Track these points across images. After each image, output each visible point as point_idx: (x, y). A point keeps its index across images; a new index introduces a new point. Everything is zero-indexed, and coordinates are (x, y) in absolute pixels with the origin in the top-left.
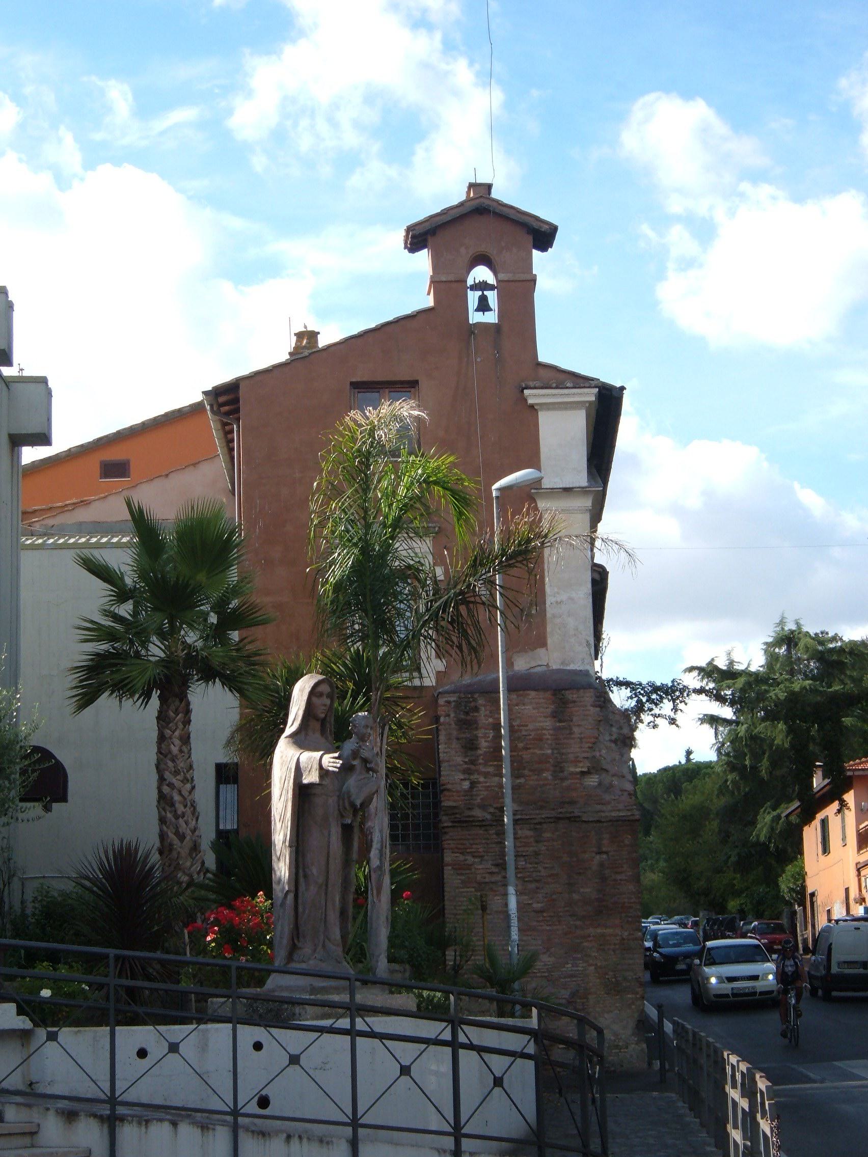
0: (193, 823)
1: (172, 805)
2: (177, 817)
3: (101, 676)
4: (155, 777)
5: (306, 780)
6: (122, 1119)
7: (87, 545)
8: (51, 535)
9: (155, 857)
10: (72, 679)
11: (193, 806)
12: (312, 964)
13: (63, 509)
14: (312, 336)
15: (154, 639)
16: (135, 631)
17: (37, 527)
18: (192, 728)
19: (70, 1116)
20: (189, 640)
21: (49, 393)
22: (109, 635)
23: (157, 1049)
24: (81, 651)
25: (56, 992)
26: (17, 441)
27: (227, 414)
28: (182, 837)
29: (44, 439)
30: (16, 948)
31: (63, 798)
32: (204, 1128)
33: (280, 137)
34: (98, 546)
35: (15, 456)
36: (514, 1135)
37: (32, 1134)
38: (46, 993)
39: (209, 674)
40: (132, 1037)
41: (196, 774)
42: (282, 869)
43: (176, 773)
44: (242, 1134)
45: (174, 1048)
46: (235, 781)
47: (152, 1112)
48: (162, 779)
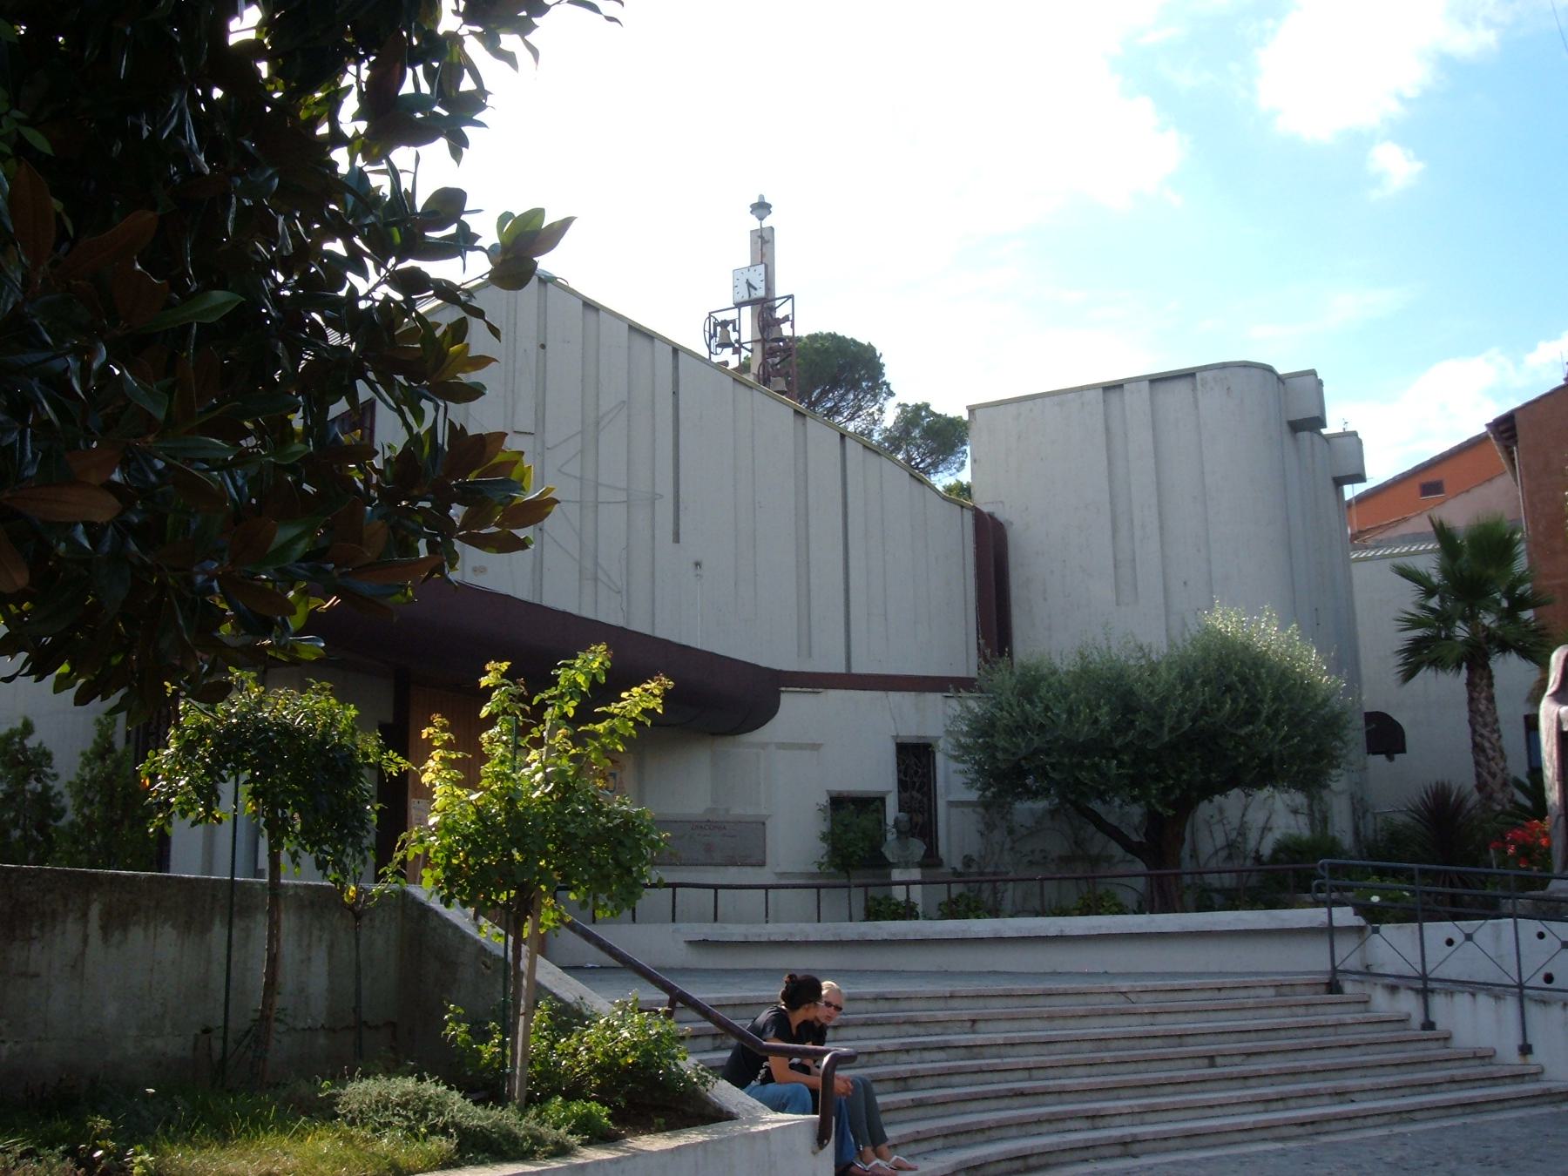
0: (1502, 765)
1: (1483, 750)
2: (1489, 760)
3: (1420, 655)
4: (1468, 729)
6: (1432, 991)
9: (1476, 796)
15: (1459, 623)
16: (1443, 618)
17: (1369, 542)
18: (1497, 690)
19: (1393, 989)
21: (1360, 442)
22: (1415, 623)
23: (1458, 938)
25: (1383, 898)
26: (1339, 482)
27: (1508, 439)
28: (1494, 776)
29: (1360, 478)
31: (1403, 750)
32: (1497, 997)
34: (1408, 554)
35: (1340, 494)
36: (1327, 939)
38: (1375, 899)
39: (1504, 647)
40: (1438, 931)
41: (1502, 726)
43: (1485, 725)
44: (1527, 1003)
45: (1469, 937)
47: (1455, 986)
48: (1474, 731)
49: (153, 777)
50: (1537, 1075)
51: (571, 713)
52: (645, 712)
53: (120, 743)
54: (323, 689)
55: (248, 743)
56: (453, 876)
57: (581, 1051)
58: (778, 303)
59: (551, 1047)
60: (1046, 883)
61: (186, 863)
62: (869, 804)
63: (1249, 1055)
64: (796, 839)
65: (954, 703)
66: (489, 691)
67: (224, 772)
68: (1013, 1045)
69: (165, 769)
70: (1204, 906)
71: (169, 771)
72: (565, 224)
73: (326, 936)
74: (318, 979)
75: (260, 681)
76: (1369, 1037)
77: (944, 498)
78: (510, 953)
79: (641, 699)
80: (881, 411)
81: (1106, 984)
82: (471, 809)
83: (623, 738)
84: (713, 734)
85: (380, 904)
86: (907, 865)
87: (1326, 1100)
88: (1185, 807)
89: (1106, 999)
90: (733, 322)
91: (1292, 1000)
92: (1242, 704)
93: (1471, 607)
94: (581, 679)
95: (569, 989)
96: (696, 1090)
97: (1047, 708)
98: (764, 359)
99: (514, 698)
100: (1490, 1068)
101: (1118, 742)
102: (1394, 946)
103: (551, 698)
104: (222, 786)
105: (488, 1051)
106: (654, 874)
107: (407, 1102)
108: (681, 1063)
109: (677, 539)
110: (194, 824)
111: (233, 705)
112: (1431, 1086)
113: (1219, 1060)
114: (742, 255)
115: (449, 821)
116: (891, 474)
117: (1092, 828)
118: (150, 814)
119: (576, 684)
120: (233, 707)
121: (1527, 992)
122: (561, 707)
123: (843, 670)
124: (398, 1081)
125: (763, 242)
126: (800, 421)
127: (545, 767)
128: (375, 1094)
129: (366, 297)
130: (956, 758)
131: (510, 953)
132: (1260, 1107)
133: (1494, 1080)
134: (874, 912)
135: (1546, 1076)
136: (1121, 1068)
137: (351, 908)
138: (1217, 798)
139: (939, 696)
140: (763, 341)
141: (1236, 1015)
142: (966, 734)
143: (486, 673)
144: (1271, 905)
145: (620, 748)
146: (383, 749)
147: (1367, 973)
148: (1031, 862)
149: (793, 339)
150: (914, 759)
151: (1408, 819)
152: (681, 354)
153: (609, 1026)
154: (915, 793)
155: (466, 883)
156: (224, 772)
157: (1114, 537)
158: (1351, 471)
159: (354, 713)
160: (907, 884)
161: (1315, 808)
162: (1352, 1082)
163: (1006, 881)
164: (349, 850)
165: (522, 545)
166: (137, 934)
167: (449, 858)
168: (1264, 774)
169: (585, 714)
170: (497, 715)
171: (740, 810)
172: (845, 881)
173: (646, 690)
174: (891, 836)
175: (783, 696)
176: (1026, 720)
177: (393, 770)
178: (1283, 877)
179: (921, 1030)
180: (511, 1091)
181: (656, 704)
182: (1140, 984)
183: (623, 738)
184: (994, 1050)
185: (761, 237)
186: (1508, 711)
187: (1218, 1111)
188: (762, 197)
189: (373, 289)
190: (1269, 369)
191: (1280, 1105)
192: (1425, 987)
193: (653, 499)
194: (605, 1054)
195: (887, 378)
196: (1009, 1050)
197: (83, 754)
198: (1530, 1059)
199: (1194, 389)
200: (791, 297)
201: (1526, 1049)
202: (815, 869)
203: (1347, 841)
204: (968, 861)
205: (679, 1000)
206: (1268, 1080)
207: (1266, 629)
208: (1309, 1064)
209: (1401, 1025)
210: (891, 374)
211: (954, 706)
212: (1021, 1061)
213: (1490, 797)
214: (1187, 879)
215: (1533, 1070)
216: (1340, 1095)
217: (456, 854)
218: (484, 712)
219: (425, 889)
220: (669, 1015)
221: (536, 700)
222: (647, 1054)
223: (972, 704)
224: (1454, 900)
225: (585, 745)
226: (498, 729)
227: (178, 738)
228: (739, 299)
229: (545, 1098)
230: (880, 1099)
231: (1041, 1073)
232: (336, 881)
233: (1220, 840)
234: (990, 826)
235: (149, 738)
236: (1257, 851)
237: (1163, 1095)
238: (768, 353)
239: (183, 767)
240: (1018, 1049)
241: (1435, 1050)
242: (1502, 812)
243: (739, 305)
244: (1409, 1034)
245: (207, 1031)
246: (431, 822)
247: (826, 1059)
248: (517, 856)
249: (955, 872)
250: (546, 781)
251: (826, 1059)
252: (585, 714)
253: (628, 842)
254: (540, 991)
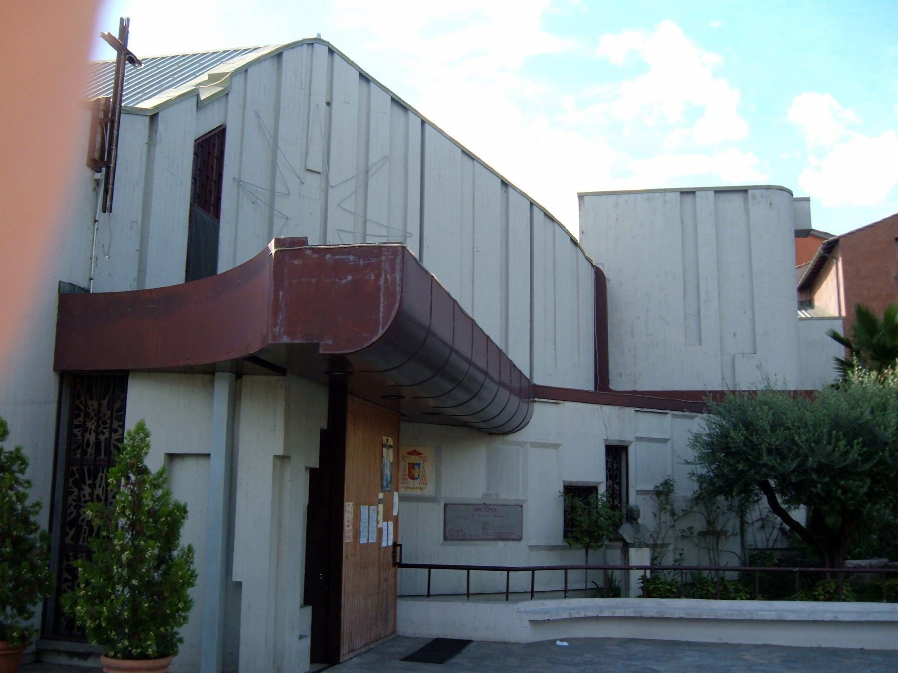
64: (543, 517)
139: (632, 410)
152: (426, 125)
171: (506, 495)
188: (319, 35)
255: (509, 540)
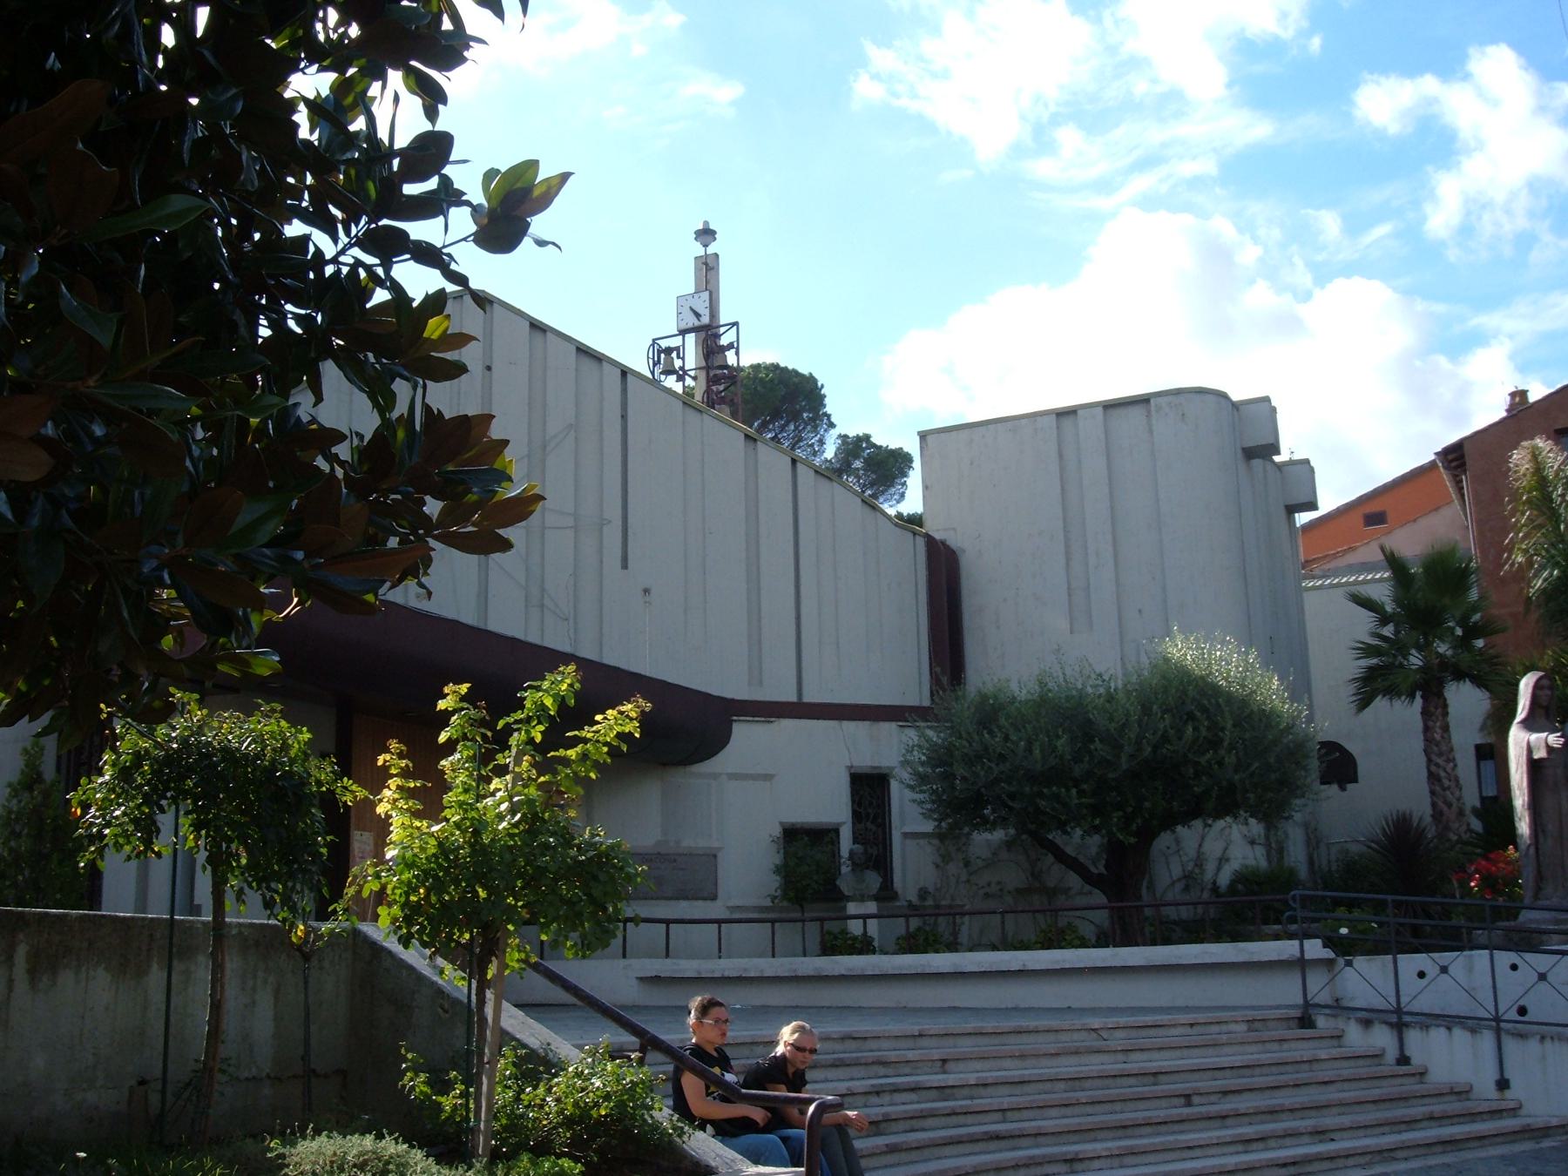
1: (1439, 780)
3: (1376, 683)
4: (1424, 759)
5: (1536, 757)
6: (1407, 1025)
7: (1356, 583)
8: (1328, 577)
10: (1352, 689)
11: (1457, 780)
12: (1555, 901)
13: (1335, 556)
14: (1523, 394)
15: (1413, 651)
18: (1451, 719)
19: (1367, 1023)
20: (1441, 650)
23: (1431, 971)
24: (1356, 666)
26: (1292, 510)
28: (1450, 805)
29: (1312, 506)
30: (1323, 898)
31: (1355, 780)
32: (1473, 1031)
33: (1466, 231)
35: (1291, 521)
37: (1339, 1037)
38: (1344, 931)
39: (1459, 676)
40: (1410, 963)
41: (1458, 756)
42: (1524, 827)
43: (1440, 754)
45: (1444, 970)
46: (1492, 757)
47: (1430, 1020)
48: (1429, 761)
49: (86, 807)
50: (1514, 1111)
51: (538, 738)
52: (620, 736)
53: (49, 770)
54: (273, 711)
55: (190, 770)
56: (412, 912)
57: (549, 1102)
58: (722, 330)
59: (517, 1099)
60: (1008, 916)
61: (118, 902)
62: (822, 836)
63: (1225, 1093)
64: (748, 871)
65: (912, 733)
66: (447, 715)
67: (164, 802)
68: (985, 1085)
69: (99, 800)
70: (1165, 938)
71: (103, 800)
72: (565, 177)
73: (271, 979)
74: (263, 1025)
75: (201, 703)
76: (1346, 1073)
77: (896, 525)
78: (474, 997)
79: (616, 722)
80: (821, 442)
81: (1078, 1022)
82: (433, 842)
83: (597, 765)
84: (664, 765)
85: (329, 944)
86: (862, 898)
87: (1306, 1139)
88: (1147, 836)
89: (1076, 1036)
90: (677, 349)
91: (1266, 1035)
92: (1204, 732)
93: (1426, 635)
94: (548, 702)
95: (531, 1032)
96: (671, 1142)
97: (1006, 738)
98: (708, 387)
99: (474, 723)
100: (1468, 1104)
101: (1077, 770)
102: (1366, 979)
103: (516, 722)
104: (160, 818)
105: (447, 1103)
106: (644, 909)
107: (365, 1163)
108: (655, 1113)
109: (625, 566)
110: (129, 858)
111: (174, 729)
112: (1410, 1123)
113: (1196, 1099)
114: (687, 282)
115: (409, 854)
116: (843, 499)
117: (1050, 858)
118: (80, 847)
119: (543, 708)
120: (172, 732)
121: (1503, 1025)
122: (528, 732)
123: (794, 699)
124: (356, 1138)
125: (708, 269)
126: (751, 444)
127: (511, 797)
128: (329, 1153)
129: (335, 261)
130: (911, 788)
131: (474, 997)
132: (1240, 1148)
133: (1473, 1116)
134: (830, 947)
135: (1523, 1112)
136: (1098, 1108)
137: (299, 948)
138: (1179, 828)
139: (893, 725)
140: (708, 368)
141: (1210, 1051)
142: (923, 764)
143: (444, 696)
144: (1235, 938)
145: (593, 775)
146: (339, 776)
147: (1338, 1007)
148: (987, 895)
149: (739, 369)
150: (869, 789)
151: (1365, 849)
153: (579, 1075)
154: (869, 825)
155: (425, 920)
156: (164, 802)
157: (1068, 564)
158: (1303, 499)
159: (307, 736)
160: (865, 917)
161: (1273, 840)
162: (1329, 1120)
163: (963, 914)
164: (298, 887)
165: (506, 545)
166: (66, 978)
167: (407, 894)
168: (1227, 805)
169: (555, 737)
170: (457, 741)
171: (691, 842)
172: (798, 915)
173: (621, 713)
174: (845, 869)
175: (735, 726)
176: (986, 749)
177: (348, 799)
178: (1245, 909)
179: (890, 1071)
180: (475, 1147)
181: (632, 727)
182: (1112, 1021)
183: (597, 765)
184: (965, 1092)
185: (706, 264)
186: (1465, 735)
187: (1198, 1152)
188: (706, 223)
189: (343, 252)
190: (1223, 396)
191: (1261, 1145)
192: (1399, 1020)
193: (602, 523)
194: (576, 1104)
195: (828, 410)
196: (982, 1091)
197: (10, 785)
198: (1508, 1094)
199: (1149, 416)
200: (736, 324)
201: (1503, 1084)
202: (768, 903)
203: (1303, 873)
204: (923, 894)
205: (650, 1043)
206: (1246, 1119)
207: (1218, 655)
208: (1287, 1102)
209: (1376, 1061)
210: (833, 405)
211: (911, 735)
212: (995, 1103)
213: (1447, 828)
214: (1148, 912)
215: (1512, 1105)
216: (1320, 1134)
217: (415, 890)
218: (443, 737)
219: (381, 930)
220: (641, 1062)
221: (501, 724)
222: (621, 1105)
223: (930, 733)
224: (1416, 931)
225: (555, 773)
226: (458, 756)
227: (114, 765)
228: (683, 326)
229: (512, 1156)
230: (858, 1144)
231: (1016, 1115)
232: (284, 920)
233: (1177, 871)
234: (946, 858)
235: (81, 764)
236: (1214, 883)
237: (1141, 1136)
238: (712, 381)
239: (119, 796)
240: (990, 1090)
241: (1410, 1086)
242: (1458, 842)
243: (683, 332)
244: (1385, 1070)
245: (142, 1083)
246: (388, 856)
247: (812, 1109)
248: (482, 894)
249: (910, 905)
250: (513, 811)
251: (812, 1109)
252: (555, 737)
253: (603, 877)
254: (505, 1037)
255: (697, 899)
